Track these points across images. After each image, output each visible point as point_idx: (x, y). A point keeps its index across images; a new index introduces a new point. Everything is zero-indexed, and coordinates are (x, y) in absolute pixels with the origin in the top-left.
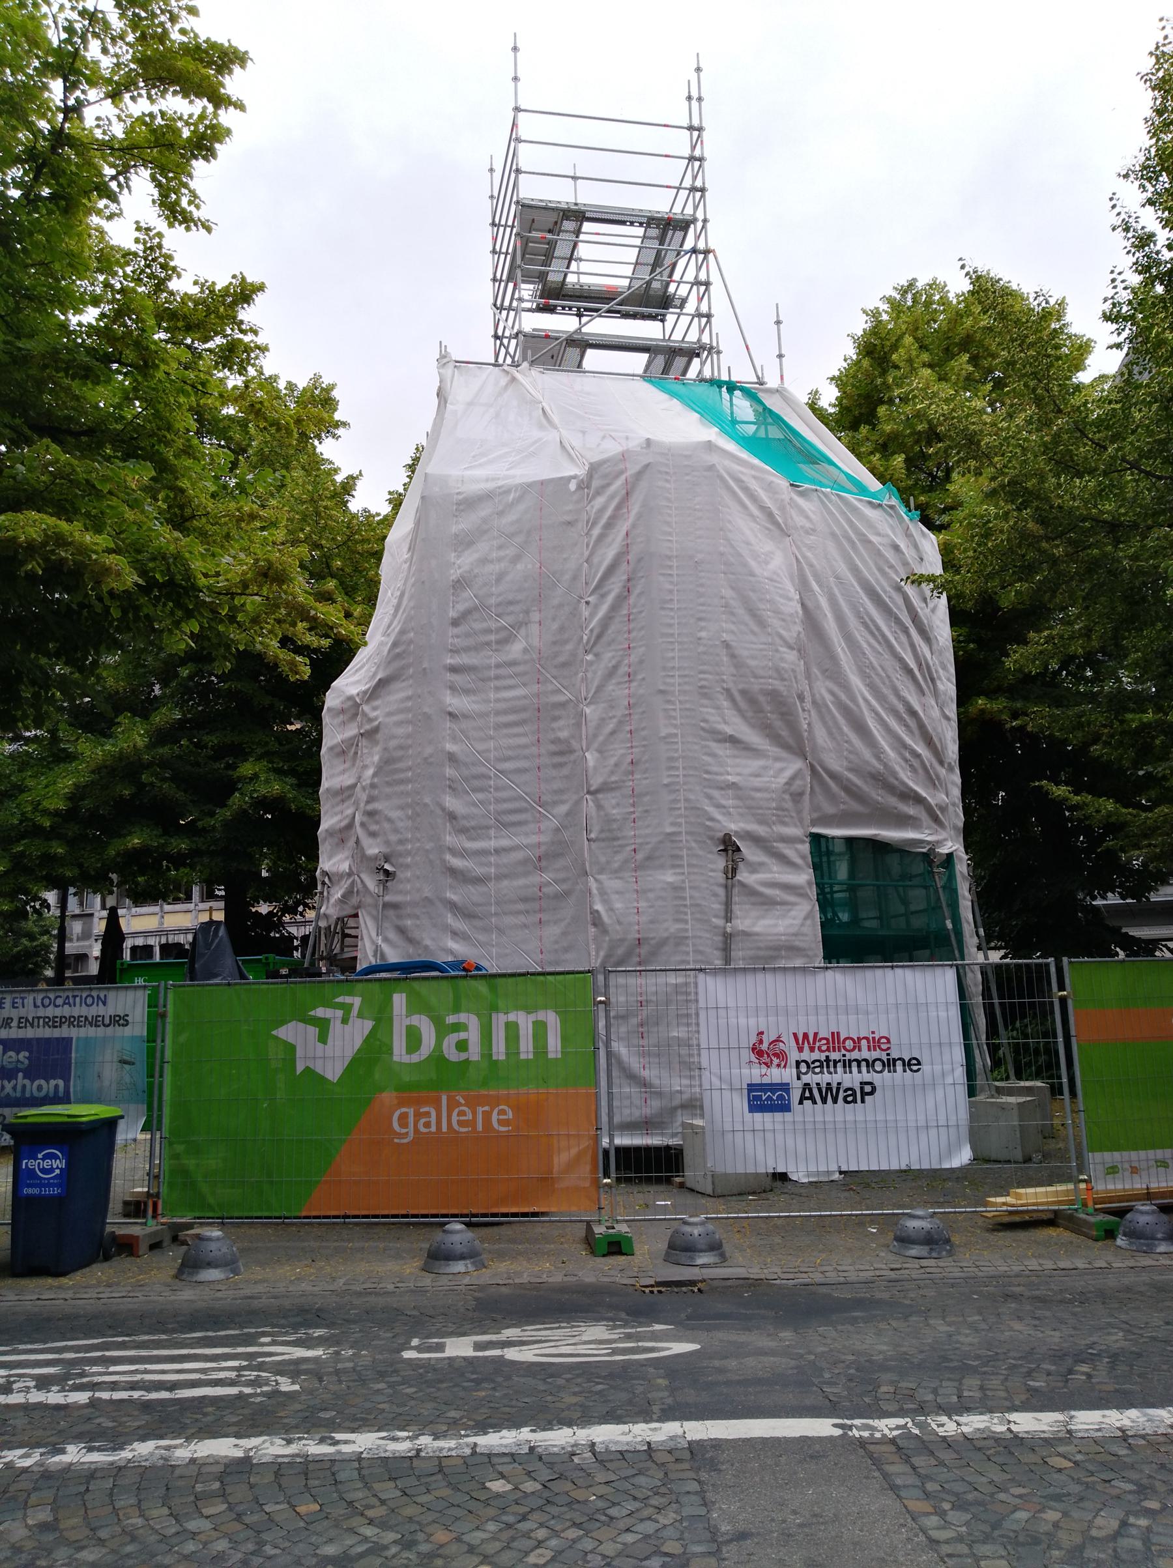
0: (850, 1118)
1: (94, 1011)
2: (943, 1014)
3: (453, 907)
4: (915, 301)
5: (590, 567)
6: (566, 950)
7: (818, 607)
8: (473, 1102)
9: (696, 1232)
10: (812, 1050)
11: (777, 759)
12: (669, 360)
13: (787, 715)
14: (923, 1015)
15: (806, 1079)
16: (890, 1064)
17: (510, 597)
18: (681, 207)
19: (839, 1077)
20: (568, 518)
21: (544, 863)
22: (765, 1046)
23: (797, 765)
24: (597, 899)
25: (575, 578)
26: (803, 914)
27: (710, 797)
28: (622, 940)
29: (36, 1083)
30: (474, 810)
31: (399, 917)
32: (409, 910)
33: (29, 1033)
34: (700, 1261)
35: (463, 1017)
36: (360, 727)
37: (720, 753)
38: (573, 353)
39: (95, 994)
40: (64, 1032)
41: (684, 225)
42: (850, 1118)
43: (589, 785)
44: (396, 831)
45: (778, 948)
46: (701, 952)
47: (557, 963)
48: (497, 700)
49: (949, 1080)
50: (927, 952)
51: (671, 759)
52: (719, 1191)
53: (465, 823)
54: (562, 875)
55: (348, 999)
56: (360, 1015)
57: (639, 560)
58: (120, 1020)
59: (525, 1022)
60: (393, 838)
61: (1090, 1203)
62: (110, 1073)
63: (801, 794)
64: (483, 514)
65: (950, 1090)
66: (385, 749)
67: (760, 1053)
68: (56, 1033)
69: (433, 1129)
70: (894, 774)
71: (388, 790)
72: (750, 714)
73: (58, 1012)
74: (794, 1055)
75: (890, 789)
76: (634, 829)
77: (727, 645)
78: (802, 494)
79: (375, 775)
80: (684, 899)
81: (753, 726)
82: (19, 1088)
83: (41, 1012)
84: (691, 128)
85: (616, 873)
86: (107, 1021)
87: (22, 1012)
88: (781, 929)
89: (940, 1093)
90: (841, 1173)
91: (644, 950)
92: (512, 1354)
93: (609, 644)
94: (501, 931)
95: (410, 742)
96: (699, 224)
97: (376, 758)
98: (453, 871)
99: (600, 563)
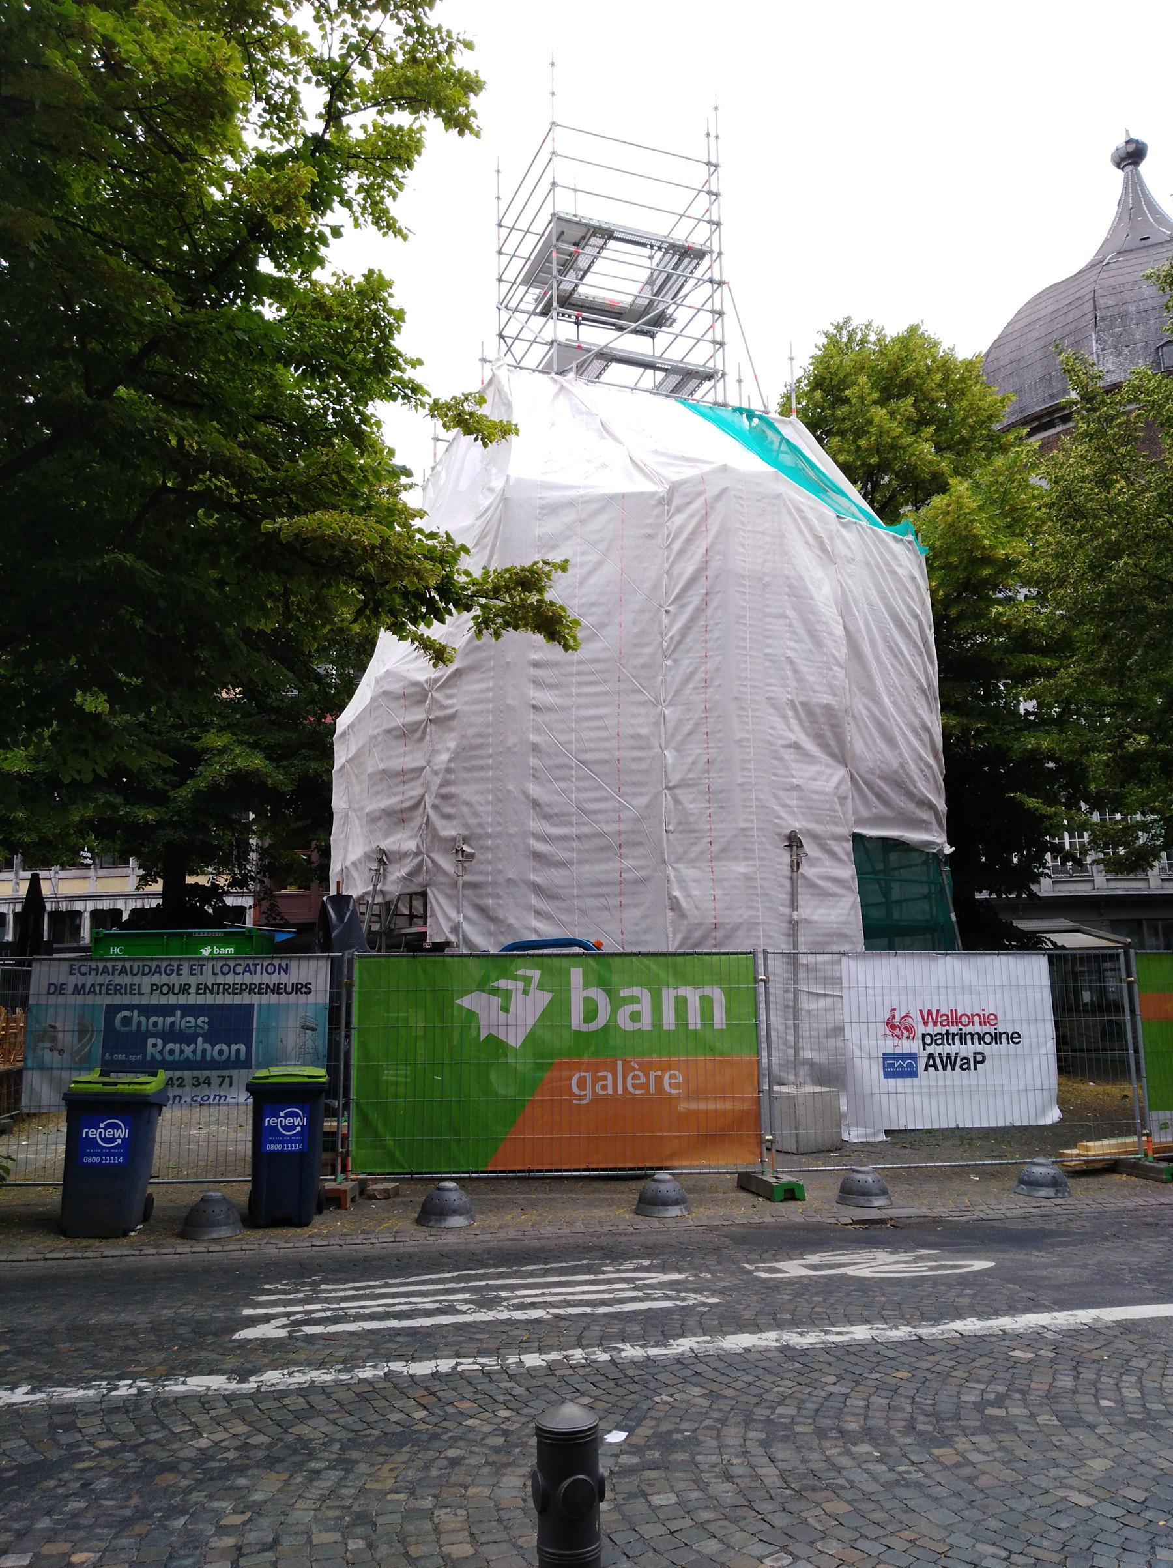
0: (965, 1082)
1: (275, 979)
2: (1038, 995)
3: (537, 889)
4: (850, 338)
5: (670, 578)
6: (646, 932)
7: (859, 630)
8: (645, 1068)
9: (870, 1179)
10: (935, 1024)
11: (827, 766)
12: (684, 380)
13: (836, 728)
14: (1022, 996)
15: (930, 1049)
16: (996, 1038)
17: (593, 598)
18: (697, 240)
19: (956, 1048)
20: (649, 531)
21: (624, 850)
22: (897, 1021)
23: (841, 772)
24: (675, 885)
25: (655, 587)
26: (849, 905)
27: (777, 797)
28: (700, 924)
29: (218, 1047)
30: (557, 798)
31: (479, 896)
32: (490, 890)
33: (209, 999)
34: (876, 1204)
35: (636, 991)
36: (429, 711)
37: (786, 757)
38: (598, 364)
39: (276, 963)
40: (246, 999)
41: (700, 255)
42: (965, 1082)
43: (668, 781)
44: (475, 814)
45: (830, 935)
46: (770, 937)
47: (637, 944)
48: (579, 695)
49: (1043, 1051)
50: (885, 941)
51: (744, 761)
52: (802, 1150)
53: (548, 810)
54: (641, 863)
55: (529, 972)
56: (541, 987)
57: (717, 577)
58: (302, 988)
59: (692, 995)
60: (472, 821)
61: (1150, 1153)
62: (292, 1039)
63: (845, 798)
64: (567, 520)
65: (1044, 1059)
66: (463, 737)
67: (893, 1027)
68: (237, 1000)
69: (610, 1091)
70: (913, 782)
71: (466, 775)
72: (807, 724)
73: (239, 979)
74: (920, 1029)
75: (910, 795)
76: (709, 823)
77: (790, 661)
78: (844, 525)
79: (450, 760)
80: (755, 888)
81: (808, 735)
82: (199, 1052)
83: (220, 979)
84: (709, 164)
85: (692, 862)
86: (289, 989)
87: (201, 979)
88: (833, 918)
89: (1036, 1062)
90: (887, 1133)
91: (719, 934)
92: (850, 1271)
93: (688, 651)
94: (583, 912)
95: (490, 731)
96: (715, 255)
97: (452, 745)
98: (537, 856)
99: (681, 574)
